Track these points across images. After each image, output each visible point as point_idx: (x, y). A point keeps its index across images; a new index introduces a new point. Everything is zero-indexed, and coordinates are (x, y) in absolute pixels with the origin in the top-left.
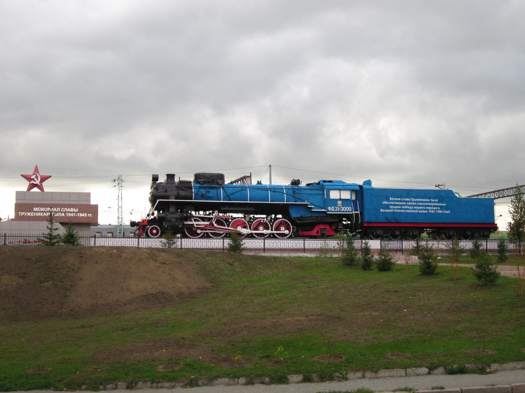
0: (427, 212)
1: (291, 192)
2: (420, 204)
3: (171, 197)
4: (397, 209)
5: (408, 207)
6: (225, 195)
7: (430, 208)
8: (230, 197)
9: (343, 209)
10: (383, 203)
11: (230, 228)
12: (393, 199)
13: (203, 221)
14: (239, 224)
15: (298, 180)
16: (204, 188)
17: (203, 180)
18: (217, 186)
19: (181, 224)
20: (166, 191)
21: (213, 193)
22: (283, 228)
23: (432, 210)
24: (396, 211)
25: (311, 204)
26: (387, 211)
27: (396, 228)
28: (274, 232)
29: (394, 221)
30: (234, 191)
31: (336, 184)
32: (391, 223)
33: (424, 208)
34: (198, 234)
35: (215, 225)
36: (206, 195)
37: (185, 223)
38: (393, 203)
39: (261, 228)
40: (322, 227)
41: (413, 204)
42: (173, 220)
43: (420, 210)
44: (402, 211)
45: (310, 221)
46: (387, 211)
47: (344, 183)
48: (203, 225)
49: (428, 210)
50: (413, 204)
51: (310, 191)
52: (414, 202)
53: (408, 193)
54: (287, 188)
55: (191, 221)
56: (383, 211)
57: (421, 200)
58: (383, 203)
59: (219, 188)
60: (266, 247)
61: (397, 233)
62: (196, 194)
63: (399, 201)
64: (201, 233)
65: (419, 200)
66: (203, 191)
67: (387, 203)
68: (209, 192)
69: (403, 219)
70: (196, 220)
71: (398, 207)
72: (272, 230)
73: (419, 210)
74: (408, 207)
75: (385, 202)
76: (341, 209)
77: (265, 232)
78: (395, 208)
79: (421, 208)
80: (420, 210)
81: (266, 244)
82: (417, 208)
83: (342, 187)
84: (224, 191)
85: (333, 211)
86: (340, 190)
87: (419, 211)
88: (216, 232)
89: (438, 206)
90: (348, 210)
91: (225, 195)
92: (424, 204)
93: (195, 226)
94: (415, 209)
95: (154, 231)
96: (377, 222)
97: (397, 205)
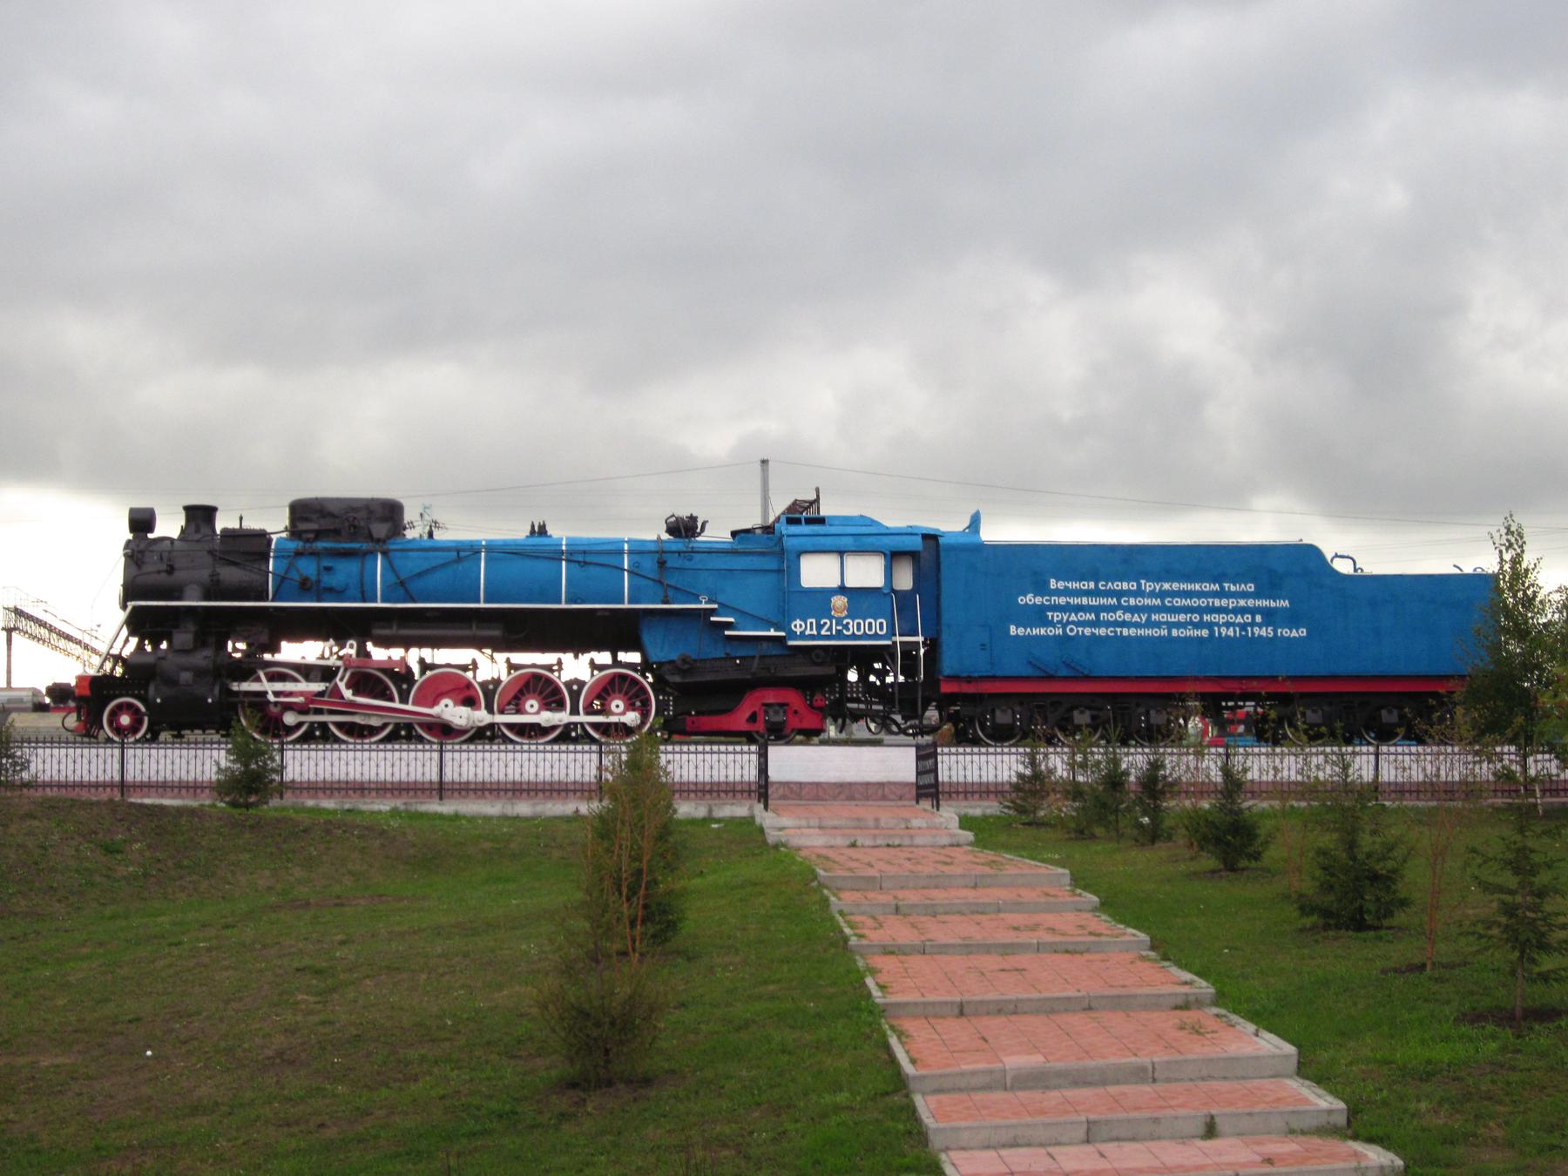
0: (1205, 633)
1: (649, 565)
2: (1178, 602)
3: (188, 591)
4: (1078, 624)
5: (1127, 617)
6: (393, 579)
7: (1222, 618)
8: (413, 587)
9: (864, 628)
10: (1022, 600)
11: (409, 707)
12: (1061, 585)
13: (308, 679)
14: (445, 688)
15: (693, 519)
16: (315, 554)
17: (314, 526)
18: (365, 546)
19: (217, 690)
20: (171, 570)
21: (345, 571)
22: (617, 705)
23: (1228, 625)
24: (1072, 631)
25: (725, 608)
26: (1036, 631)
27: (1080, 701)
28: (582, 718)
29: (1064, 672)
30: (426, 566)
31: (833, 530)
32: (1050, 678)
33: (1196, 618)
34: (290, 730)
35: (348, 694)
36: (319, 581)
37: (235, 687)
38: (1062, 601)
39: (532, 704)
40: (771, 696)
41: (1147, 601)
42: (186, 677)
43: (1178, 625)
44: (1102, 631)
45: (720, 677)
46: (1036, 631)
47: (873, 522)
48: (301, 694)
49: (1210, 626)
50: (1147, 601)
51: (728, 558)
52: (1152, 594)
53: (1125, 561)
54: (639, 550)
55: (258, 680)
56: (1021, 631)
57: (1184, 586)
58: (1022, 600)
59: (372, 553)
60: (448, 777)
61: (1389, 717)
62: (281, 580)
63: (1088, 593)
64: (300, 725)
65: (1175, 586)
66: (308, 567)
67: (1038, 600)
68: (328, 569)
69: (1105, 664)
70: (272, 678)
71: (1082, 616)
72: (575, 711)
73: (1170, 625)
74: (1127, 617)
75: (1030, 599)
76: (846, 627)
77: (547, 718)
78: (1069, 618)
79: (1182, 617)
80: (1178, 625)
81: (130, 767)
82: (1164, 617)
83: (857, 538)
84: (390, 566)
85: (812, 637)
86: (841, 553)
87: (1175, 633)
88: (357, 719)
89: (1253, 611)
90: (870, 630)
91: (393, 579)
92: (1195, 602)
93: (271, 698)
94: (1158, 625)
95: (125, 720)
96: (994, 678)
97: (1079, 608)
